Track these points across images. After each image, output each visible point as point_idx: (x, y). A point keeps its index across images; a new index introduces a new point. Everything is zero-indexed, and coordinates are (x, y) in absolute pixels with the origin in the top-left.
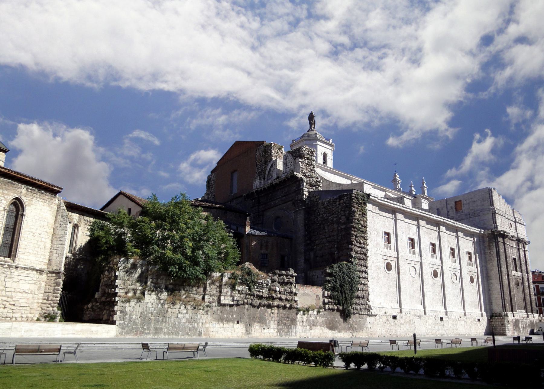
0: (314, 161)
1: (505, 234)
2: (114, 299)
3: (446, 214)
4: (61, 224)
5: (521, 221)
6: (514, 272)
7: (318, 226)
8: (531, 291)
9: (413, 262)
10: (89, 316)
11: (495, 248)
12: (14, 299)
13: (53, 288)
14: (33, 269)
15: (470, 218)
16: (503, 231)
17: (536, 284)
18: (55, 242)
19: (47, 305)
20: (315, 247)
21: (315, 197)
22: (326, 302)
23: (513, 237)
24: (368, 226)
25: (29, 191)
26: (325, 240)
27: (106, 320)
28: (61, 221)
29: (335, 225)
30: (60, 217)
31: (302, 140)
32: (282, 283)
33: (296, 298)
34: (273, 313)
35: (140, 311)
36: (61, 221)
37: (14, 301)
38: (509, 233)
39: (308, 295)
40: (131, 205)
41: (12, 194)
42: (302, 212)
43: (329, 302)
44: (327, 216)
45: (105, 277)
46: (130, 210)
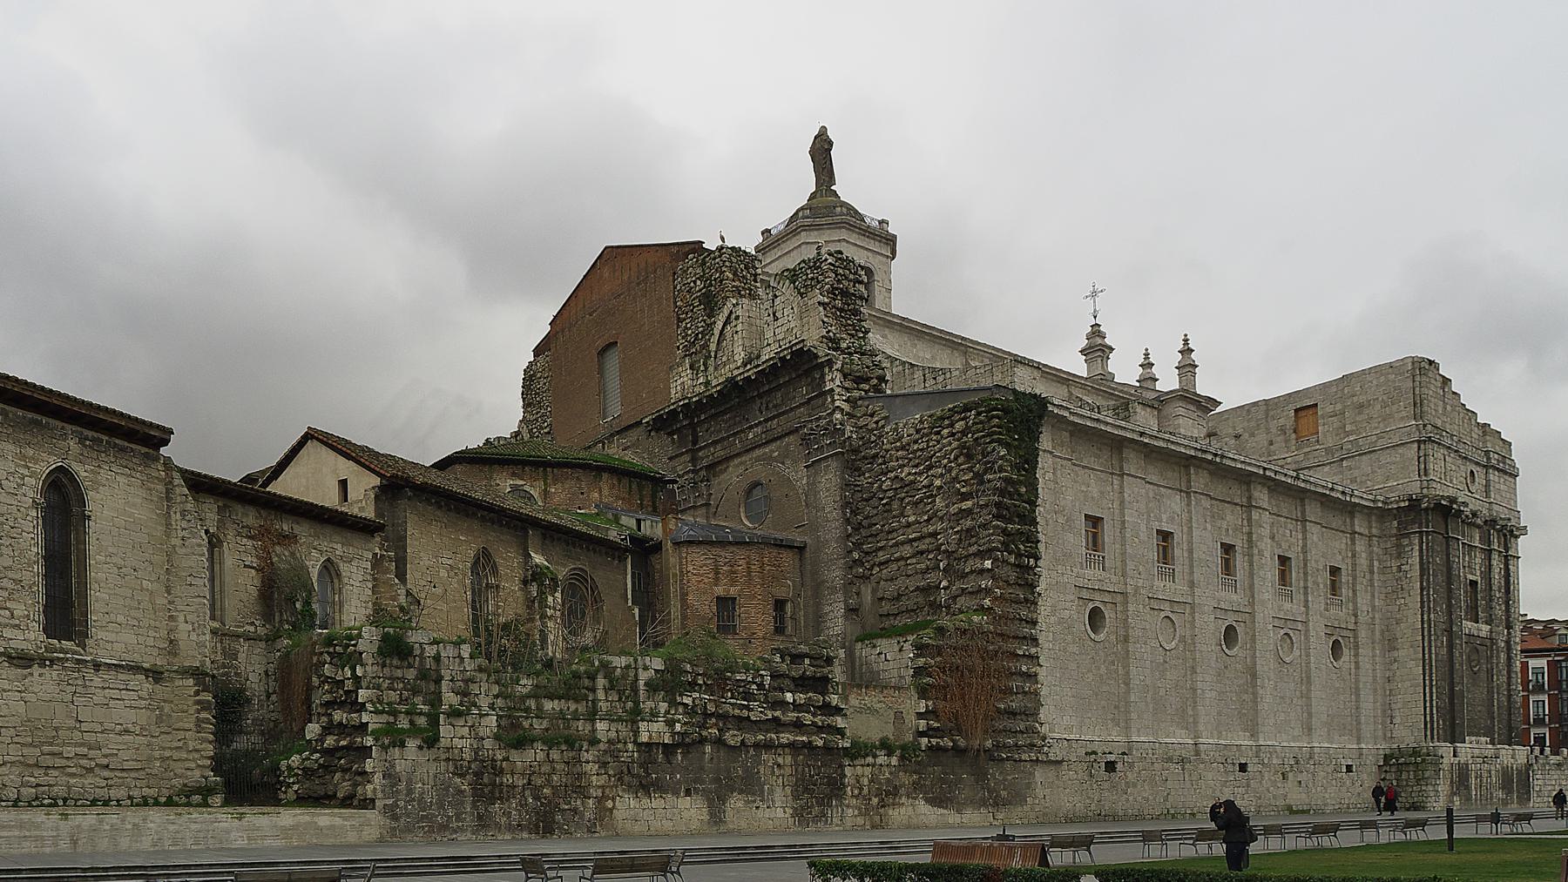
0: (861, 298)
1: (1455, 506)
5: (1504, 463)
6: (1468, 626)
8: (1514, 680)
9: (1166, 606)
10: (296, 787)
13: (193, 719)
14: (135, 669)
15: (1342, 460)
17: (1550, 656)
18: (177, 591)
19: (188, 765)
23: (1474, 514)
24: (1039, 501)
25: (85, 446)
27: (345, 798)
28: (183, 529)
36: (183, 529)
37: (106, 756)
38: (1465, 504)
39: (872, 711)
40: (346, 468)
42: (834, 464)
43: (930, 728)
46: (343, 484)
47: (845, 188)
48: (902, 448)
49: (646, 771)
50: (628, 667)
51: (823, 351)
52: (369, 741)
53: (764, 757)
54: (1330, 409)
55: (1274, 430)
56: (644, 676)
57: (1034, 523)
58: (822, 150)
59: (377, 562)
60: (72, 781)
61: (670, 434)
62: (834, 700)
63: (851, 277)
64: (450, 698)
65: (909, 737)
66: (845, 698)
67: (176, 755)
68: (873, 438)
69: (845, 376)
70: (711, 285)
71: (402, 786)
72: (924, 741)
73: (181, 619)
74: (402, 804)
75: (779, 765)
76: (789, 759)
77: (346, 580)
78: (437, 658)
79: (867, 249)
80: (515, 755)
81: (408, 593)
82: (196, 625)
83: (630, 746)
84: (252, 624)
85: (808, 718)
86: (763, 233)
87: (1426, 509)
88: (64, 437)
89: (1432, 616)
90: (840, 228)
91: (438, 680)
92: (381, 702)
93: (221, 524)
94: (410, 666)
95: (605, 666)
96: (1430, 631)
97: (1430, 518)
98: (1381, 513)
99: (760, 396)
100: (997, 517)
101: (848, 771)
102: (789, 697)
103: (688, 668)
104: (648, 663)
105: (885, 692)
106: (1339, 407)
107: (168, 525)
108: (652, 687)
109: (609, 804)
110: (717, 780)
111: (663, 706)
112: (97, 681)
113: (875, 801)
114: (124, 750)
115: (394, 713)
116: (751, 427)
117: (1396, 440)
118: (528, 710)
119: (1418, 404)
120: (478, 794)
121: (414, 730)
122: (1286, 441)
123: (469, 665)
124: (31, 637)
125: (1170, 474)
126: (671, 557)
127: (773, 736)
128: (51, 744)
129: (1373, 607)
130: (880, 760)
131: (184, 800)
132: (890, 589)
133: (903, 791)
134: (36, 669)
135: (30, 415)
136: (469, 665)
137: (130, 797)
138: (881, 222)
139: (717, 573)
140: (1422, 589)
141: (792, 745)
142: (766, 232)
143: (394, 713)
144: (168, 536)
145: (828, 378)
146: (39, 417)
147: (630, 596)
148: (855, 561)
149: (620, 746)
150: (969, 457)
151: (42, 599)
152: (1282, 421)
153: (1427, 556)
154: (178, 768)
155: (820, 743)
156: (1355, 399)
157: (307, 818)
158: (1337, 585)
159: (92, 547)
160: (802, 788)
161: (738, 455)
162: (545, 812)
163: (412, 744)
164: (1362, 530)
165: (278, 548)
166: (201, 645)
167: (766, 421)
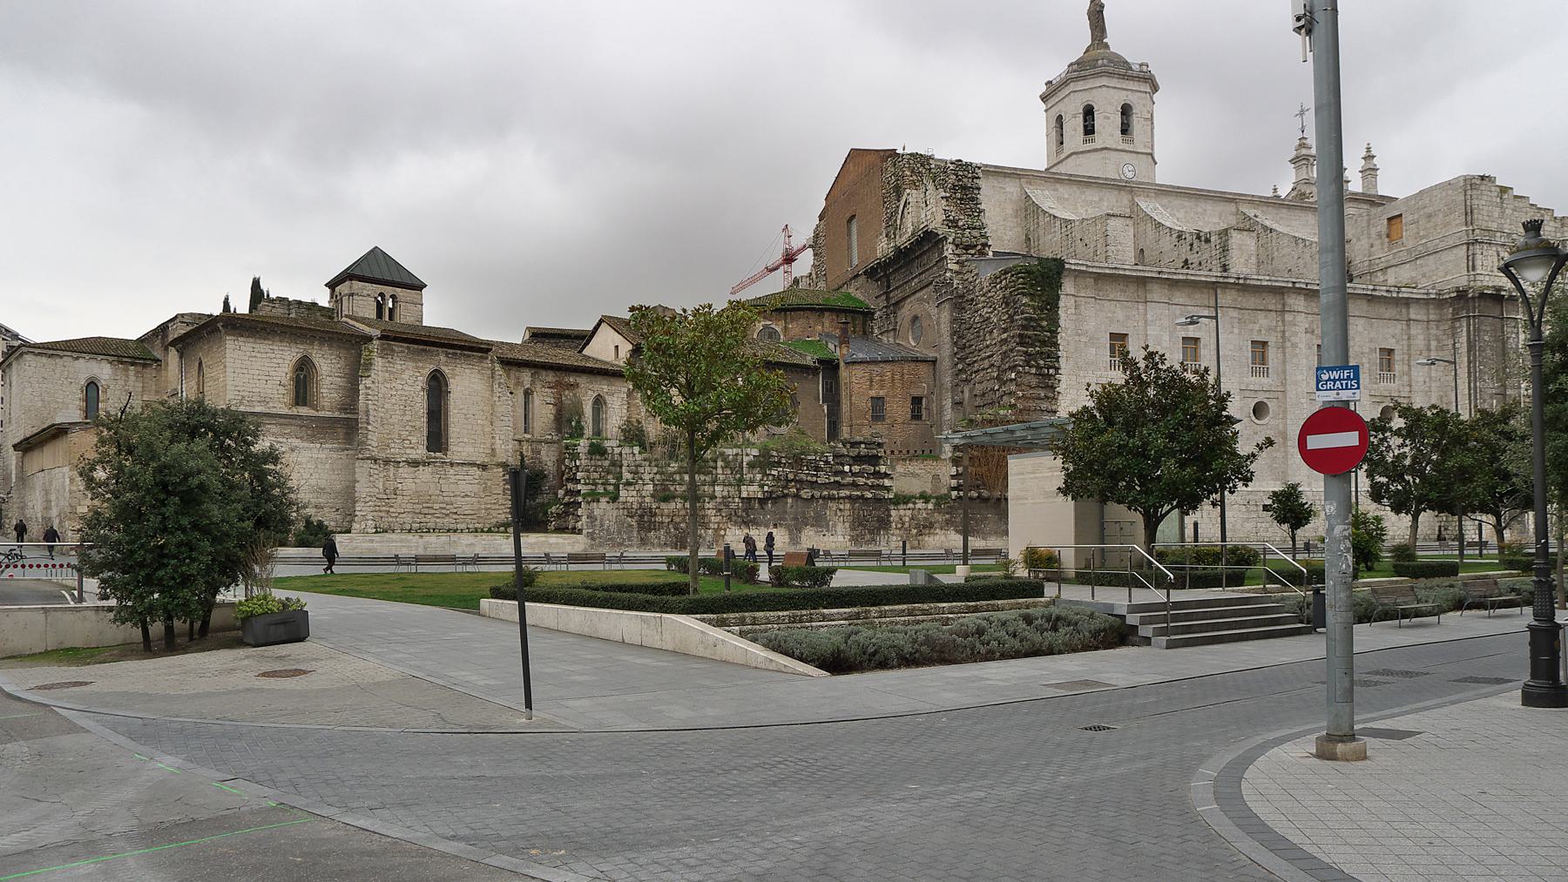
3: (1366, 252)
11: (1465, 334)
14: (473, 464)
16: (1494, 287)
35: (615, 515)
39: (914, 475)
47: (1116, 41)
48: (984, 295)
49: (747, 514)
50: (737, 455)
51: (942, 231)
52: (580, 499)
53: (830, 504)
54: (1411, 218)
55: (1373, 235)
56: (746, 459)
57: (1056, 345)
60: (438, 520)
61: (877, 281)
62: (883, 469)
63: (970, 175)
64: (627, 476)
65: (944, 491)
66: (893, 468)
67: (493, 507)
68: (971, 288)
69: (957, 246)
70: (898, 180)
71: (598, 523)
72: (954, 493)
74: (597, 532)
75: (840, 510)
76: (848, 506)
78: (621, 454)
79: (1125, 89)
80: (663, 505)
83: (737, 500)
85: (861, 481)
86: (1046, 84)
87: (1473, 298)
88: (438, 355)
89: (1478, 384)
90: (1101, 76)
91: (621, 467)
92: (589, 479)
93: (533, 382)
94: (606, 459)
95: (722, 454)
96: (1476, 396)
97: (1477, 305)
98: (1439, 302)
99: (917, 257)
100: (1021, 344)
101: (893, 513)
102: (847, 468)
103: (775, 453)
104: (749, 452)
105: (925, 462)
106: (1416, 216)
108: (751, 465)
109: (722, 532)
110: (796, 519)
111: (759, 477)
113: (914, 531)
114: (466, 505)
115: (595, 484)
116: (913, 279)
117: (1451, 243)
118: (674, 480)
119: (1469, 213)
120: (641, 527)
121: (606, 493)
122: (1382, 244)
123: (638, 457)
124: (420, 452)
125: (1198, 296)
126: (844, 373)
128: (428, 503)
129: (1431, 378)
130: (918, 506)
131: (496, 530)
132: (979, 388)
133: (937, 525)
134: (421, 468)
135: (421, 347)
136: (638, 457)
137: (468, 528)
138: (1141, 65)
139: (872, 382)
140: (1469, 362)
141: (849, 497)
142: (1049, 83)
143: (595, 484)
144: (492, 396)
146: (425, 347)
147: (821, 398)
148: (960, 370)
149: (729, 499)
150: (1007, 304)
151: (425, 433)
152: (1379, 228)
153: (1474, 335)
154: (494, 513)
155: (870, 496)
156: (1426, 210)
157: (544, 539)
158: (1392, 362)
159: (451, 408)
160: (858, 523)
161: (909, 296)
162: (681, 537)
163: (603, 500)
164: (1419, 317)
165: (567, 392)
166: (507, 451)
167: (920, 274)
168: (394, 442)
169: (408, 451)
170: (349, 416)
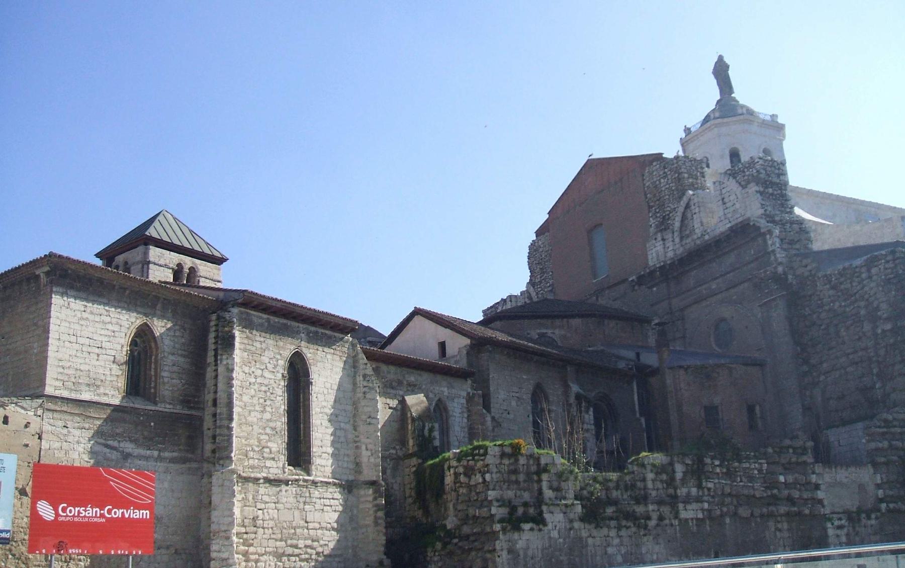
2: (855, 513)
4: (364, 393)
7: (823, 330)
12: (322, 542)
13: (372, 518)
20: (822, 378)
21: (806, 266)
22: (880, 497)
26: (843, 359)
28: (365, 387)
29: (865, 324)
30: (361, 378)
31: (709, 127)
32: (788, 468)
33: (820, 494)
34: (780, 530)
40: (444, 334)
41: (289, 346)
44: (840, 306)
45: (459, 487)
46: (442, 345)
47: (742, 95)
51: (763, 223)
58: (721, 71)
59: (470, 399)
73: (364, 447)
76: (785, 526)
77: (451, 413)
81: (493, 418)
82: (373, 451)
84: (394, 448)
107: (355, 384)
112: (316, 494)
124: (278, 466)
127: (774, 509)
141: (788, 514)
145: (770, 242)
168: (253, 450)
169: (269, 463)
170: (193, 412)
